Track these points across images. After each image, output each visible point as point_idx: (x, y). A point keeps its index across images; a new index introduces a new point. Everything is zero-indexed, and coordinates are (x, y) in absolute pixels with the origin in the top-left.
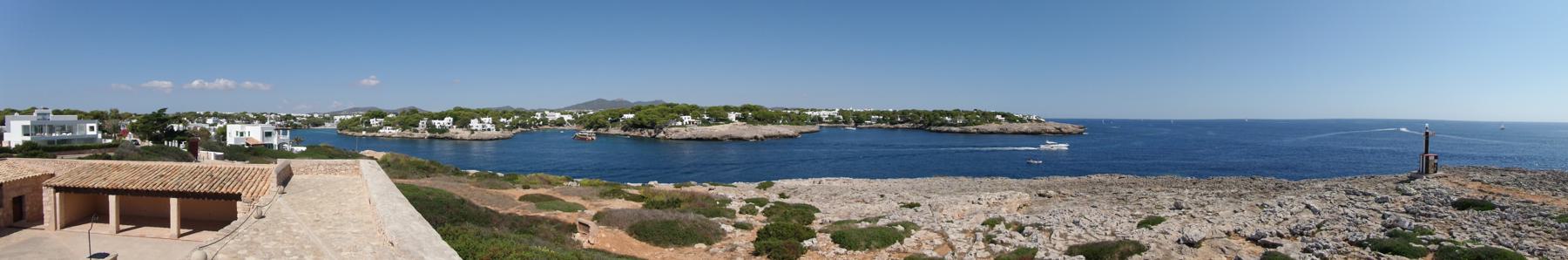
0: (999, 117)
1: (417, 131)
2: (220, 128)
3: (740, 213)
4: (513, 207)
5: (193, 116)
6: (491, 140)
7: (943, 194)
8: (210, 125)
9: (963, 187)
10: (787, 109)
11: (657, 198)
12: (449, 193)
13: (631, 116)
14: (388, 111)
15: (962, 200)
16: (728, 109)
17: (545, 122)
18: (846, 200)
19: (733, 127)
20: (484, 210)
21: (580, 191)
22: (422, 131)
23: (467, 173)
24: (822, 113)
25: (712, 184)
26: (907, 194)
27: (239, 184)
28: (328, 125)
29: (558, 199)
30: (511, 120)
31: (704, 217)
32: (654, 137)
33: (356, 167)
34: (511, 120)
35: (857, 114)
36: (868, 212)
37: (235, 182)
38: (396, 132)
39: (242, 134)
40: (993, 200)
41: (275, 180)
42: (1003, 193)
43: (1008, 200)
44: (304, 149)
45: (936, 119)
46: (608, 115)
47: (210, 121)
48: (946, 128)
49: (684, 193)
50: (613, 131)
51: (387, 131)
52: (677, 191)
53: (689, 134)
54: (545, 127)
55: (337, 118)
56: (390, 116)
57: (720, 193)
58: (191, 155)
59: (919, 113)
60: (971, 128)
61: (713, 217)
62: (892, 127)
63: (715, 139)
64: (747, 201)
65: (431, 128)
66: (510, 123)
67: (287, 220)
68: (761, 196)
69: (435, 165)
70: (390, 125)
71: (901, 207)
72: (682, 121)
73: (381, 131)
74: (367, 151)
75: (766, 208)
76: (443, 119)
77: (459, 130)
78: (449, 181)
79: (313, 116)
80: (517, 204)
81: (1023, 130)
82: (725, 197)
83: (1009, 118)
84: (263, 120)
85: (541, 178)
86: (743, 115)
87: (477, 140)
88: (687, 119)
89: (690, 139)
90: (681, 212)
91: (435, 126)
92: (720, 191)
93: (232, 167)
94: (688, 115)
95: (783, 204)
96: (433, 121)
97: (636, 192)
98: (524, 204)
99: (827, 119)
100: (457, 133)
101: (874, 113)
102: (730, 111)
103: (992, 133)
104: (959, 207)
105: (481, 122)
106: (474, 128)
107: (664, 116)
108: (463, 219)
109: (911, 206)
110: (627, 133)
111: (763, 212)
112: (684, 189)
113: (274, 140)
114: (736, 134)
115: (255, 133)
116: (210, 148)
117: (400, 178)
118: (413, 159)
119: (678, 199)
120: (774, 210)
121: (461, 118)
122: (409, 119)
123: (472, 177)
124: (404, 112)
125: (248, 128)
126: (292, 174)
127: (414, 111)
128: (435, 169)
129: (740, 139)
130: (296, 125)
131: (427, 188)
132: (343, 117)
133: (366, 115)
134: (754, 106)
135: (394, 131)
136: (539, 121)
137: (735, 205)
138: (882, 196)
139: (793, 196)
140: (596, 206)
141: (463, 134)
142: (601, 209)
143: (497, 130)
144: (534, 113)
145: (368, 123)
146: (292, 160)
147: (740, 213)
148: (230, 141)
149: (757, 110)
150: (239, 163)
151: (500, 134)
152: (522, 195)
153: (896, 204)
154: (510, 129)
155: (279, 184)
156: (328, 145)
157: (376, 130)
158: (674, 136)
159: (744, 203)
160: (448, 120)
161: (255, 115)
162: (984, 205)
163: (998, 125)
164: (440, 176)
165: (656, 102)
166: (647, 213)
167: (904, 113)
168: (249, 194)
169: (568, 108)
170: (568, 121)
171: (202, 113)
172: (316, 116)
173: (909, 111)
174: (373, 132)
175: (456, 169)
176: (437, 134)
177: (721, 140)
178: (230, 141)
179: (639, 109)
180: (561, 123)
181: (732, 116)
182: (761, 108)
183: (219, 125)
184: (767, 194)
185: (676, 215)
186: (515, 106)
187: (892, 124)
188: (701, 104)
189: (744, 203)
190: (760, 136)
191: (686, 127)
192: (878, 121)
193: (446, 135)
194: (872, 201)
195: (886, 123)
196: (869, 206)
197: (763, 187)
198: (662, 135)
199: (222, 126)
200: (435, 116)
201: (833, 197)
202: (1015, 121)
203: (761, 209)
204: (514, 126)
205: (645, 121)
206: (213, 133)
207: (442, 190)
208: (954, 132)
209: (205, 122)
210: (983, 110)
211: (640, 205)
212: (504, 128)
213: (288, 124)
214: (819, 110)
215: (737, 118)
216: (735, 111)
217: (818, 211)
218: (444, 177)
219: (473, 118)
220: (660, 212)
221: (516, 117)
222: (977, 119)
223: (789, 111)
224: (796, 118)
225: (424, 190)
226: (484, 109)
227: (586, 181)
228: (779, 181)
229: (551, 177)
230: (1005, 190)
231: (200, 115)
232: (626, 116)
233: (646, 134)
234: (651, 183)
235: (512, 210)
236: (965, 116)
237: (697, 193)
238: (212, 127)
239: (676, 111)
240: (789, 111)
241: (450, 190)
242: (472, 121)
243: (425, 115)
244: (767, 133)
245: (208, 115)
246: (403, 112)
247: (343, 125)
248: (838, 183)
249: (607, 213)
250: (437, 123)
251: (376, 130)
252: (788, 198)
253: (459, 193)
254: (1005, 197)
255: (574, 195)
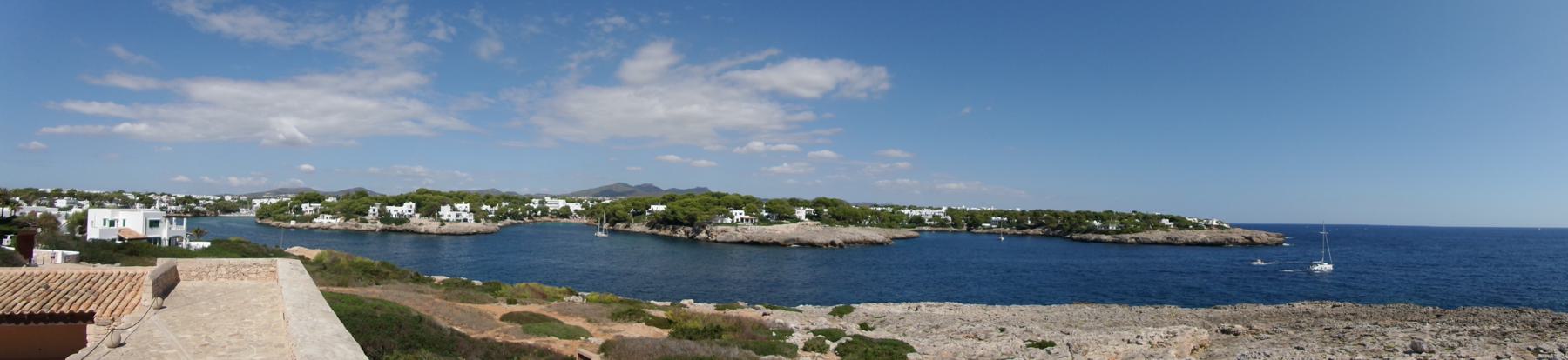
0: (1166, 222)
1: (366, 222)
2: (76, 214)
3: (805, 349)
4: (491, 329)
5: (32, 195)
6: (468, 234)
7: (1088, 329)
8: (61, 209)
9: (1116, 319)
10: (875, 206)
11: (690, 324)
12: (404, 307)
13: (662, 208)
14: (327, 193)
15: (1113, 339)
16: (795, 203)
17: (545, 212)
18: (953, 335)
19: (802, 228)
20: (449, 333)
21: (584, 310)
22: (372, 222)
23: (431, 280)
24: (923, 212)
25: (767, 307)
26: (1036, 327)
27: (93, 297)
28: (244, 212)
29: (554, 320)
30: (496, 208)
31: (754, 354)
32: (692, 237)
33: (272, 269)
34: (496, 208)
35: (972, 213)
36: (981, 352)
37: (85, 296)
38: (336, 222)
39: (112, 223)
40: (1157, 338)
41: (150, 289)
42: (1172, 329)
43: (1178, 339)
44: (207, 244)
45: (1081, 223)
46: (629, 204)
47: (61, 203)
48: (1093, 237)
49: (727, 318)
50: (637, 227)
51: (324, 220)
52: (718, 315)
53: (740, 236)
54: (545, 218)
55: (257, 202)
56: (330, 200)
57: (778, 320)
58: (20, 257)
59: (1056, 215)
60: (1128, 237)
61: (765, 355)
62: (1019, 232)
63: (776, 244)
64: (816, 332)
65: (385, 217)
66: (496, 212)
67: (160, 347)
68: (835, 326)
69: (388, 268)
70: (328, 213)
71: (1028, 346)
72: (732, 217)
73: (316, 220)
74: (296, 248)
75: (841, 344)
76: (401, 205)
77: (425, 221)
78: (406, 290)
79: (222, 199)
80: (498, 326)
81: (1198, 240)
82: (785, 326)
83: (1180, 223)
84: (147, 202)
85: (533, 290)
86: (816, 211)
87: (449, 234)
88: (738, 214)
89: (741, 243)
90: (721, 345)
91: (389, 214)
92: (778, 317)
93: (84, 272)
94: (741, 209)
95: (863, 338)
96: (388, 208)
97: (661, 314)
98: (508, 325)
99: (930, 220)
100: (420, 224)
101: (995, 213)
102: (799, 206)
103: (1156, 243)
104: (1110, 348)
105: (454, 210)
106: (445, 218)
107: (707, 210)
108: (418, 345)
109: (1042, 345)
110: (655, 231)
111: (836, 349)
112: (729, 312)
113: (164, 233)
114: (805, 237)
115: (133, 222)
116: (56, 243)
117: (339, 285)
118: (358, 259)
119: (718, 327)
120: (850, 347)
121: (428, 204)
122: (355, 203)
123: (438, 286)
124: (348, 195)
125: (122, 215)
126: (178, 280)
127: (362, 193)
128: (387, 274)
129: (812, 245)
130: (198, 211)
131: (374, 299)
132: (265, 201)
133: (297, 198)
134: (832, 200)
135: (333, 221)
136: (536, 211)
137: (798, 339)
138: (1002, 330)
139: (878, 328)
140: (605, 332)
141: (430, 225)
142: (610, 337)
143: (477, 221)
144: (529, 199)
145: (299, 210)
146: (179, 260)
147: (805, 349)
148: (93, 233)
149: (836, 206)
150: (105, 266)
151: (481, 226)
152: (505, 312)
153: (1021, 343)
154: (495, 220)
155: (155, 294)
156: (242, 239)
157: (310, 219)
158: (720, 237)
159: (811, 336)
160: (408, 206)
161: (138, 195)
162: (1145, 346)
163: (1165, 233)
164: (394, 284)
165: (698, 189)
166: (674, 344)
167: (1036, 214)
168: (107, 312)
169: (577, 194)
170: (576, 211)
171: (49, 191)
172: (228, 198)
173: (1042, 212)
174: (306, 221)
175: (417, 274)
176: (394, 226)
177: (784, 246)
178: (93, 233)
179: (672, 199)
180: (565, 213)
181: (801, 213)
182: (842, 202)
183: (75, 210)
184: (843, 323)
185: (714, 348)
186: (505, 190)
187: (1019, 228)
188: (757, 195)
189: (811, 336)
190: (838, 241)
191: (737, 226)
192: (1000, 224)
193: (405, 226)
194: (988, 337)
195: (1011, 227)
196: (983, 344)
197: (839, 313)
198: (703, 235)
199: (80, 210)
200: (390, 201)
201: (934, 331)
202: (1187, 227)
203: (833, 345)
204: (500, 216)
205: (681, 216)
206: (64, 222)
207: (395, 303)
208: (1105, 242)
209: (52, 205)
210: (1145, 212)
211: (665, 333)
212: (487, 219)
213: (188, 209)
214: (920, 208)
215: (807, 216)
216: (805, 207)
217: (912, 350)
218: (399, 284)
219: (444, 204)
220: (692, 344)
221: (504, 204)
222: (1137, 224)
223: (879, 209)
224: (889, 219)
225: (370, 302)
226: (459, 192)
227: (594, 296)
228: (861, 305)
229: (547, 289)
230: (1174, 324)
231: (44, 194)
232: (654, 208)
233: (681, 233)
234: (685, 302)
235: (489, 334)
236: (1120, 219)
237: (747, 319)
238: (64, 213)
239: (723, 203)
240: (879, 209)
241: (406, 303)
242: (442, 208)
243: (377, 199)
244: (848, 238)
245: (58, 194)
246: (347, 195)
247: (264, 212)
248: (941, 310)
249: (618, 343)
250: (394, 211)
251: (310, 219)
252: (871, 329)
253: (418, 308)
254: (1175, 335)
255: (576, 315)
